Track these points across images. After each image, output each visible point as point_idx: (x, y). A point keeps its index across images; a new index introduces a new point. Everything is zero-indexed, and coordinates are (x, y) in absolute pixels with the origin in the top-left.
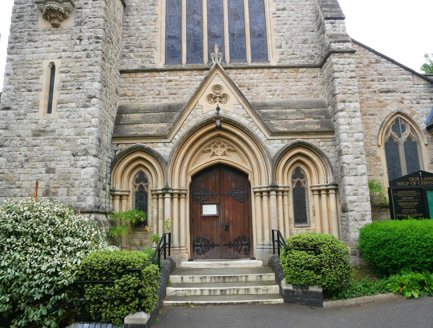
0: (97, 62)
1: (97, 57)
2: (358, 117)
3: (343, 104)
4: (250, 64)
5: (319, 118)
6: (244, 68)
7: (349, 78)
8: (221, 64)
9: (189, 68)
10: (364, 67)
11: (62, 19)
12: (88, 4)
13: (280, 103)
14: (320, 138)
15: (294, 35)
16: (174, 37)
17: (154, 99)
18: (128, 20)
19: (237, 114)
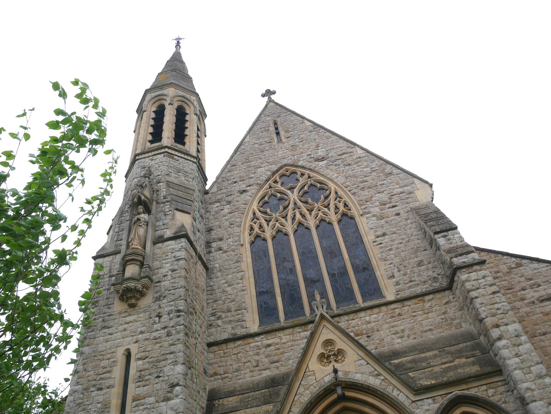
0: (179, 339)
1: (179, 333)
2: (525, 342)
3: (497, 329)
4: (361, 303)
5: (473, 356)
6: (356, 312)
7: (491, 294)
8: (327, 313)
9: (289, 325)
10: (505, 276)
11: (139, 297)
12: (167, 275)
13: (414, 346)
14: (486, 384)
15: (405, 259)
16: (267, 292)
17: (251, 374)
18: (212, 284)
19: (362, 373)
